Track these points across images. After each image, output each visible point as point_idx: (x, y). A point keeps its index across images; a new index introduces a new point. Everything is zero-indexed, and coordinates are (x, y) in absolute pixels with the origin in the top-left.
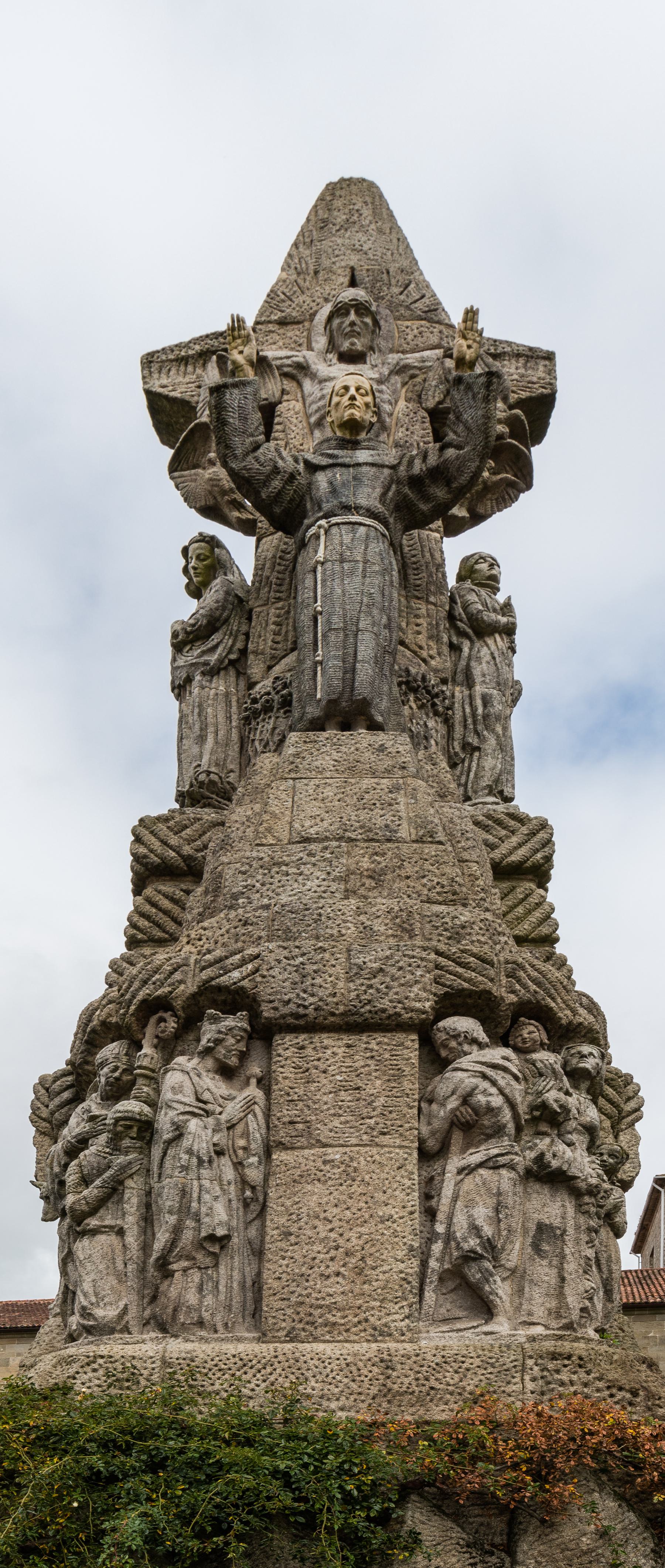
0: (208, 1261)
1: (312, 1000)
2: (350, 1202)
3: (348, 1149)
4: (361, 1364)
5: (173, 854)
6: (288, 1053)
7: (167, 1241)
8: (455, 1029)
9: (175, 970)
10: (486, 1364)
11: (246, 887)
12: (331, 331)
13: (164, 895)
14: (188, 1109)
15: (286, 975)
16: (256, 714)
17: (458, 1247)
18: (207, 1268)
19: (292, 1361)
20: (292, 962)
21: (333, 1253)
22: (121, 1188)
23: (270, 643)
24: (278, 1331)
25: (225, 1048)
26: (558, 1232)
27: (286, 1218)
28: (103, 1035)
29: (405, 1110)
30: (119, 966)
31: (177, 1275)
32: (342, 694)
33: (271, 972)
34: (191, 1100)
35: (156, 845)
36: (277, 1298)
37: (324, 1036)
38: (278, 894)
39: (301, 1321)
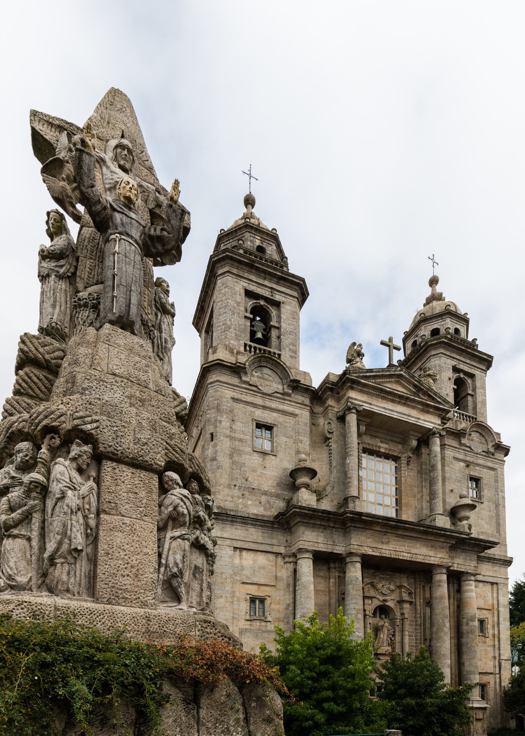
0: (72, 561)
1: (120, 448)
2: (133, 544)
3: (132, 520)
4: (138, 618)
5: (41, 356)
6: (109, 470)
7: (55, 548)
8: (172, 477)
9: (62, 415)
10: (184, 622)
11: (89, 386)
12: (116, 153)
13: (34, 374)
14: (68, 485)
15: (110, 434)
16: (80, 306)
17: (170, 571)
18: (71, 564)
19: (111, 613)
20: (112, 428)
21: (126, 565)
22: (30, 516)
23: (86, 276)
24: (103, 598)
25: (82, 459)
26: (201, 570)
27: (107, 546)
28: (17, 436)
29: (153, 507)
30: (12, 402)
31: (58, 565)
32: (124, 314)
33: (104, 430)
34: (68, 481)
35: (33, 349)
36: (103, 583)
37: (123, 466)
38: (103, 395)
39: (113, 595)
